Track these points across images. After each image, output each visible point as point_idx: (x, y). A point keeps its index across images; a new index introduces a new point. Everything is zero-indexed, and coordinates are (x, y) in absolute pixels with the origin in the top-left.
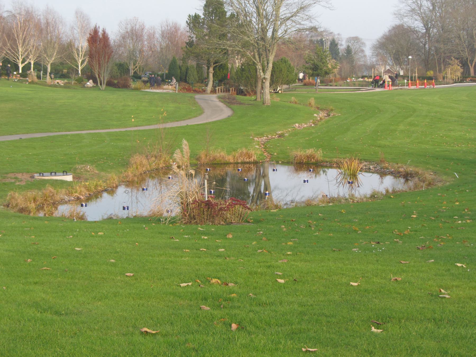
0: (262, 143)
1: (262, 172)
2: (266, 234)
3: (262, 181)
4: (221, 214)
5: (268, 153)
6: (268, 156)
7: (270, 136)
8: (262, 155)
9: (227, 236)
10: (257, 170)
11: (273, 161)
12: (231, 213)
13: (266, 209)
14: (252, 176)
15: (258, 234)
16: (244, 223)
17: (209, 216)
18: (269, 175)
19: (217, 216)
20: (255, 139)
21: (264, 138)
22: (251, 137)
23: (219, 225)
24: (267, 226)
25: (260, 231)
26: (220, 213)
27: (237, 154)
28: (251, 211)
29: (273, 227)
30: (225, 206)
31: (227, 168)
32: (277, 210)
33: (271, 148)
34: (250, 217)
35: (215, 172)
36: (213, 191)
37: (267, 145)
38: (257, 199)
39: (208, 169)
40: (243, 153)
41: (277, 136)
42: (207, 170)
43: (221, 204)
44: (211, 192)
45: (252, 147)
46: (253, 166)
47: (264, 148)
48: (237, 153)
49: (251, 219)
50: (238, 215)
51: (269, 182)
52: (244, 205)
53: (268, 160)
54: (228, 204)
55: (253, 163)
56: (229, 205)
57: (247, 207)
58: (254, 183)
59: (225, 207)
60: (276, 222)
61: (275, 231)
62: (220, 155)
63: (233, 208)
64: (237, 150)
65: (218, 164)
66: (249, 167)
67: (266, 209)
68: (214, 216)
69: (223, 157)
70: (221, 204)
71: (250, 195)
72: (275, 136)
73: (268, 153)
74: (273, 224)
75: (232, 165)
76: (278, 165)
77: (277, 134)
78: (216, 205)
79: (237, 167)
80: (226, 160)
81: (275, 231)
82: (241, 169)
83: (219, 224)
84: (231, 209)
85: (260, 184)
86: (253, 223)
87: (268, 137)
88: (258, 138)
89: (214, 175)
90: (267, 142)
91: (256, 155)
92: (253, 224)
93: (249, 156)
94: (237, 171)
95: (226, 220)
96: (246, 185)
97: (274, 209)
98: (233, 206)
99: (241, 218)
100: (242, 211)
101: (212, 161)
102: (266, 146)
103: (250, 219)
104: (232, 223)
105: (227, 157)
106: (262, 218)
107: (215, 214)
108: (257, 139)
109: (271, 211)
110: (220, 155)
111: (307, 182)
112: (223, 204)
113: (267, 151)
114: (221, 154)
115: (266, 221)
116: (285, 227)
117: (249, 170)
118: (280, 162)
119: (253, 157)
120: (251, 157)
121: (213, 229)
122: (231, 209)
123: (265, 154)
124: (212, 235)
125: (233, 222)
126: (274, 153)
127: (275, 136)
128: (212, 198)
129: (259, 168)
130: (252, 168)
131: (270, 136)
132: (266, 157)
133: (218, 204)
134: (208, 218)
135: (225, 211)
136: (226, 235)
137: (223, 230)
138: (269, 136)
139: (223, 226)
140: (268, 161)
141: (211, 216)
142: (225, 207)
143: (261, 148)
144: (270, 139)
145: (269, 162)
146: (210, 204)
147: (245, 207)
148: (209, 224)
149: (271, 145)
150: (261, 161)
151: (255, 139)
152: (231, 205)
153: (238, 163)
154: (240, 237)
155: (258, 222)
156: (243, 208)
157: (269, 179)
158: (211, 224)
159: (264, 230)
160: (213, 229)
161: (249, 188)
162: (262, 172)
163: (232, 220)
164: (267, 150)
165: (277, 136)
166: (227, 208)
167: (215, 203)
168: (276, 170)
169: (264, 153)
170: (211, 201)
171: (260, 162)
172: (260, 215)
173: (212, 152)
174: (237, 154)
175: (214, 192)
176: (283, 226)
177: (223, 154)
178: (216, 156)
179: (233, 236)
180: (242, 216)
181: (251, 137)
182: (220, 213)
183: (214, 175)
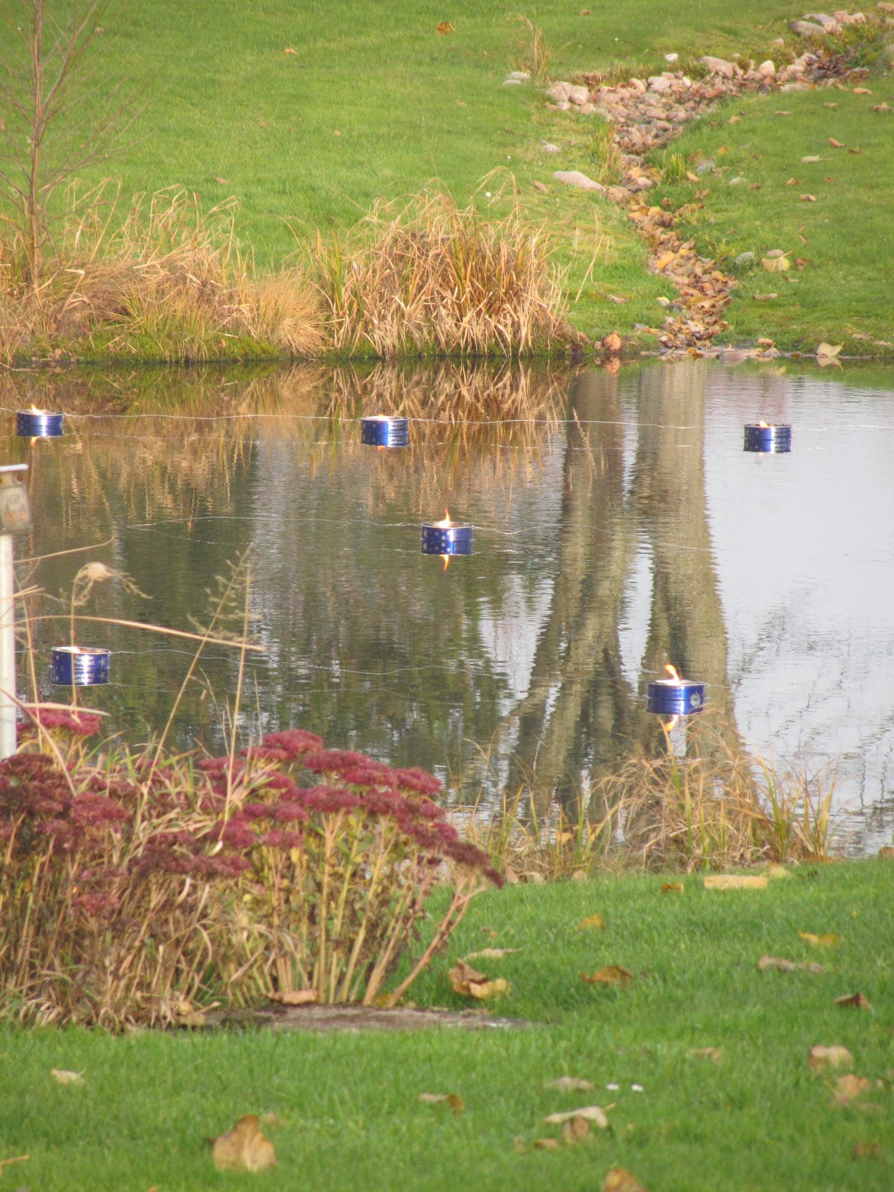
0: (636, 135)
1: (629, 458)
2: (640, 1140)
3: (629, 551)
4: (167, 905)
5: (699, 251)
6: (697, 282)
7: (726, 67)
8: (638, 270)
9: (222, 1153)
10: (571, 431)
11: (746, 338)
12: (275, 898)
13: (656, 864)
14: (528, 504)
15: (554, 1131)
16: (408, 1012)
17: (27, 930)
18: (709, 477)
19: (118, 929)
20: (562, 90)
21: (661, 82)
22: (518, 77)
23: (135, 1031)
24: (663, 1049)
25: (579, 1098)
26: (156, 899)
27: (357, 259)
28: (496, 878)
29: (719, 1056)
30: (208, 825)
31: (244, 410)
32: (779, 871)
33: (729, 193)
34: (481, 943)
35: (116, 454)
36: (86, 662)
37: (688, 158)
38: (576, 756)
39: (43, 417)
40: (424, 251)
41: (798, 66)
42: (27, 425)
43: (162, 804)
44: (64, 663)
45: (524, 186)
46: (533, 389)
47: (656, 199)
48: (357, 243)
49: (488, 972)
50: (353, 920)
51: (710, 580)
52: (412, 810)
53: (696, 327)
54: (236, 797)
55: (533, 358)
56: (250, 813)
57: (447, 834)
58: (548, 585)
59: (212, 838)
60: (755, 1010)
61: (738, 1103)
62: (171, 267)
63: (287, 844)
64: (354, 218)
65: (152, 363)
66: (494, 405)
67: (656, 864)
68: (80, 934)
69: (205, 295)
70: (162, 804)
71: (506, 707)
72: (782, 60)
73: (699, 251)
74: (729, 1031)
75: (301, 374)
76: (814, 388)
77: (810, 42)
78: (108, 815)
79: (357, 405)
80: (237, 325)
81: (738, 1103)
82: (402, 428)
83: (140, 1016)
84: (272, 857)
85: (604, 589)
86: (512, 1015)
87: (699, 74)
88: (589, 82)
89: (107, 480)
90: (693, 126)
91: (562, 270)
92: (505, 1025)
93: (488, 281)
94: (353, 446)
95: (212, 974)
96: (461, 601)
97: (742, 864)
98: (291, 828)
99: (384, 958)
100: (392, 877)
101: (81, 330)
102: (673, 177)
103: (479, 965)
104: (280, 1007)
105: (245, 287)
106: (608, 957)
107: (97, 911)
108: (582, 93)
109: (713, 881)
110: (171, 267)
111: (890, 68)
112: (189, 804)
113: (684, 231)
114: (185, 255)
115: (653, 988)
116: (858, 1067)
117: (486, 432)
118: (828, 353)
119: (532, 294)
120: (515, 294)
121: (65, 1076)
122: (272, 857)
123: (667, 257)
124: (54, 1141)
125: (290, 996)
126: (764, 249)
127: (782, 60)
128: (66, 728)
129: (606, 412)
130: (515, 413)
131: (726, 67)
132: (672, 292)
133: (131, 797)
134: (23, 955)
135: (211, 875)
136: (210, 1143)
137: (177, 1089)
138: (712, 62)
139: (184, 1040)
140: (692, 341)
141: (53, 926)
142: (212, 838)
143: (618, 192)
144: (720, 97)
145: (709, 352)
146: (46, 795)
147: (426, 841)
148: (29, 1020)
149: (732, 164)
150: (616, 342)
151: (562, 90)
152: (271, 814)
153: (376, 358)
154: (354, 1157)
155: (567, 1004)
156: (397, 851)
157: (704, 536)
158: (46, 1017)
159: (626, 1091)
160: (65, 1076)
161: (486, 627)
162: (629, 458)
163: (285, 980)
164: (690, 213)
165: (798, 66)
166: (231, 841)
167: (96, 785)
168: (785, 435)
169: (656, 246)
170: (60, 764)
171: (608, 355)
172: (593, 922)
173: (90, 233)
174: (357, 259)
175: (97, 672)
176: (837, 1053)
177: (209, 257)
178: (131, 275)
179: (279, 1155)
180: (396, 930)
181: (518, 77)
182: (156, 899)
183: (107, 480)
